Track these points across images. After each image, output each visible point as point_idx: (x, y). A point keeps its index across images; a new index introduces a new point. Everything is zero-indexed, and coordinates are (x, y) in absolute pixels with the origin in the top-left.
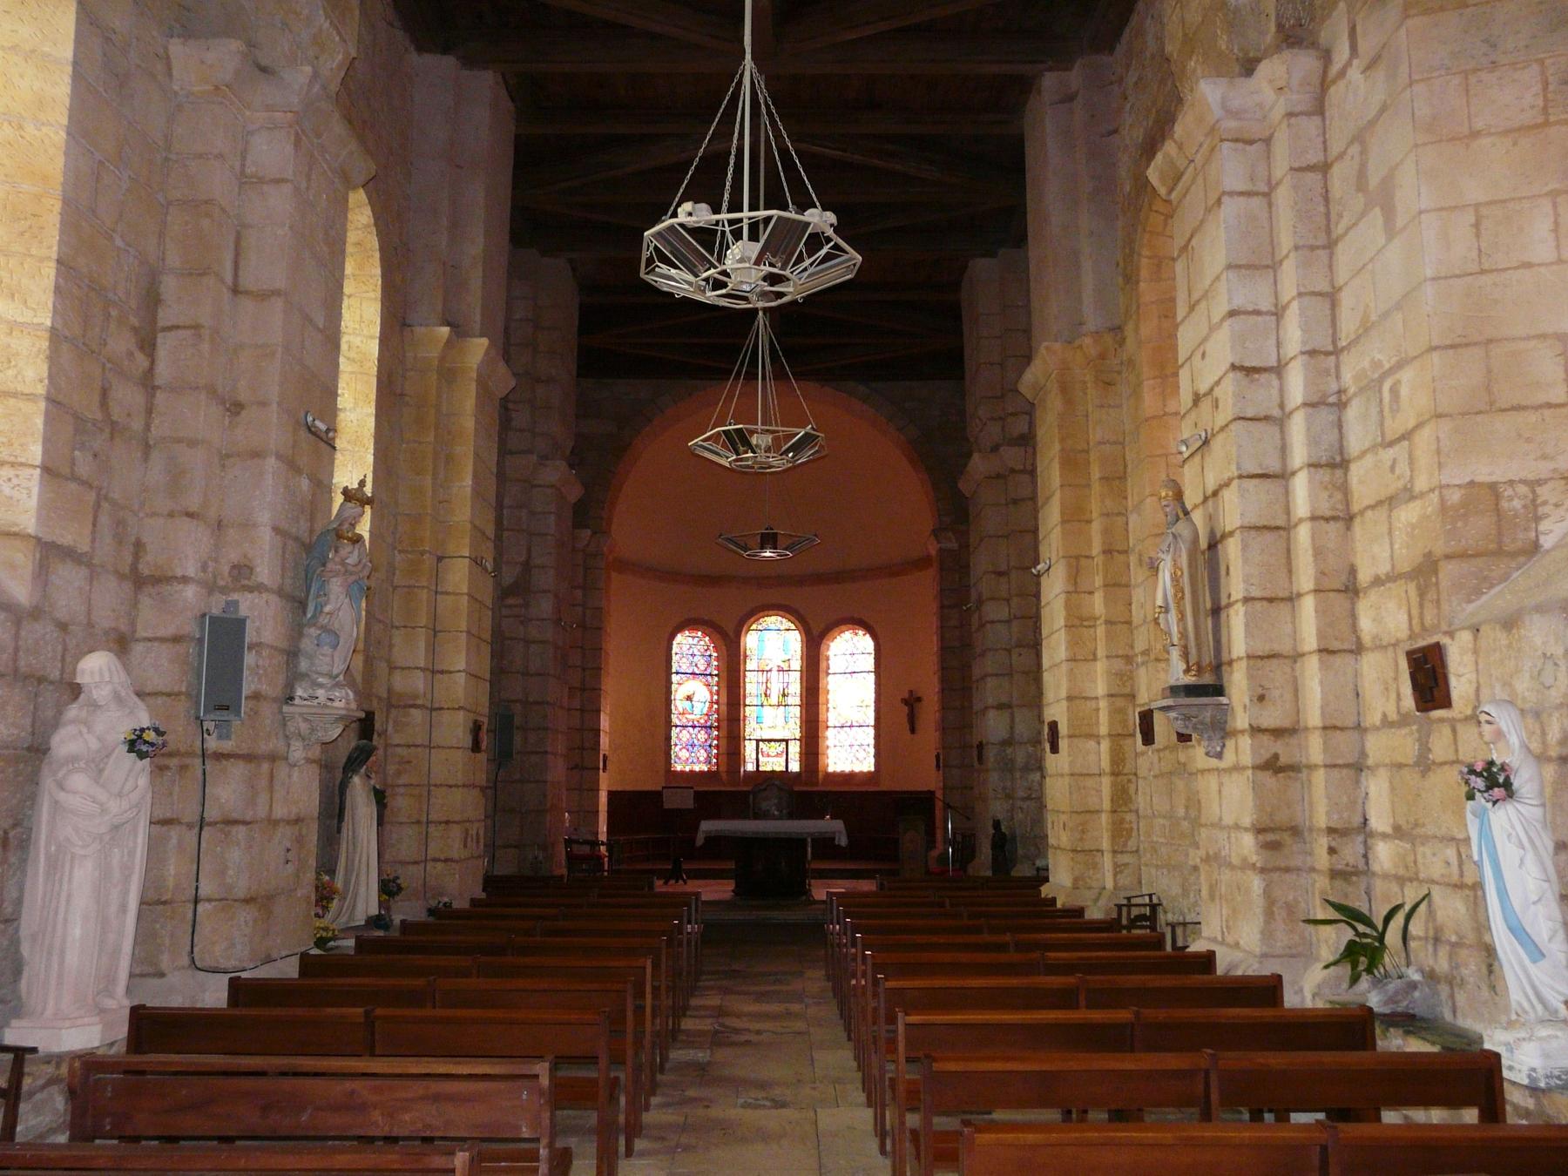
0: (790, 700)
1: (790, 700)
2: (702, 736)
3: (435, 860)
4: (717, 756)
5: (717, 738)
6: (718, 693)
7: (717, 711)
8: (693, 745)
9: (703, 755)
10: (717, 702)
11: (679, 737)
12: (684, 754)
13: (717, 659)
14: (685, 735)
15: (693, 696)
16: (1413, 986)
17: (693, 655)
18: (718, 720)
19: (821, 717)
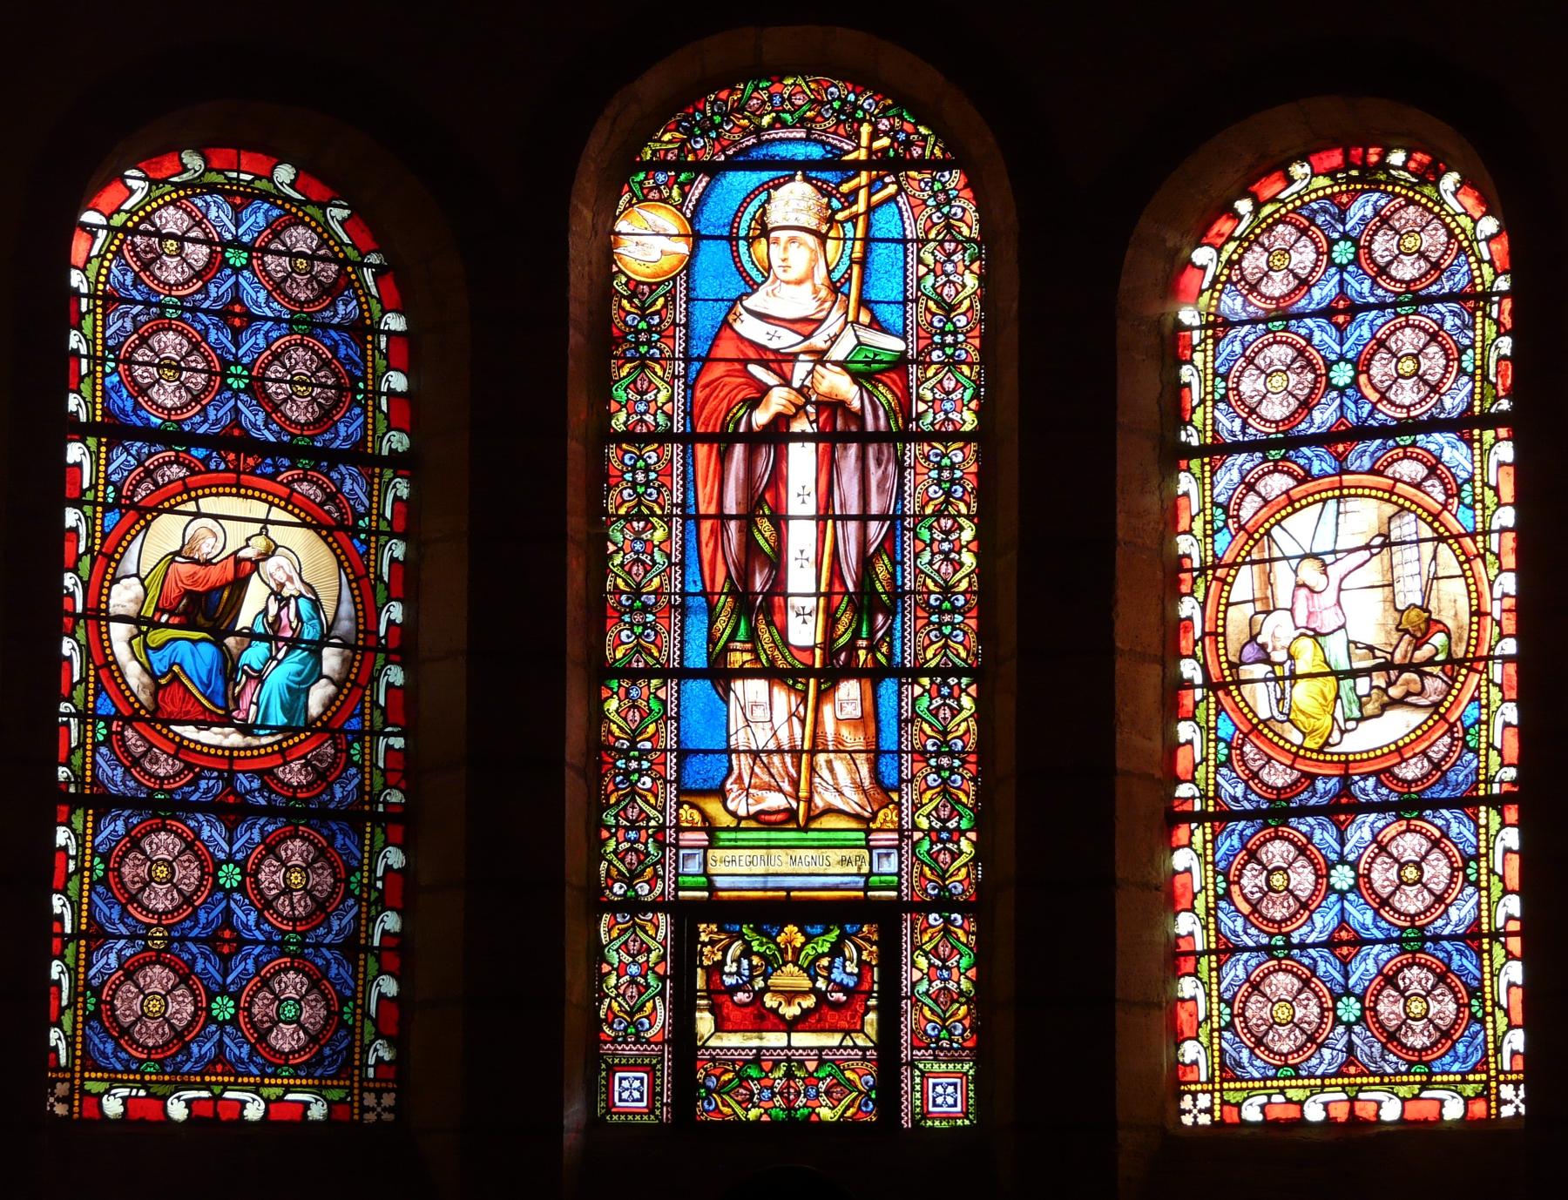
0: (914, 640)
1: (914, 640)
2: (290, 871)
3: (900, 743)
4: (398, 1020)
5: (403, 891)
6: (408, 582)
7: (406, 705)
8: (224, 941)
9: (291, 1012)
10: (403, 646)
11: (115, 880)
12: (158, 1001)
13: (407, 351)
14: (164, 868)
15: (231, 580)
16: (108, 720)
17: (235, 316)
18: (404, 768)
19: (1132, 746)
